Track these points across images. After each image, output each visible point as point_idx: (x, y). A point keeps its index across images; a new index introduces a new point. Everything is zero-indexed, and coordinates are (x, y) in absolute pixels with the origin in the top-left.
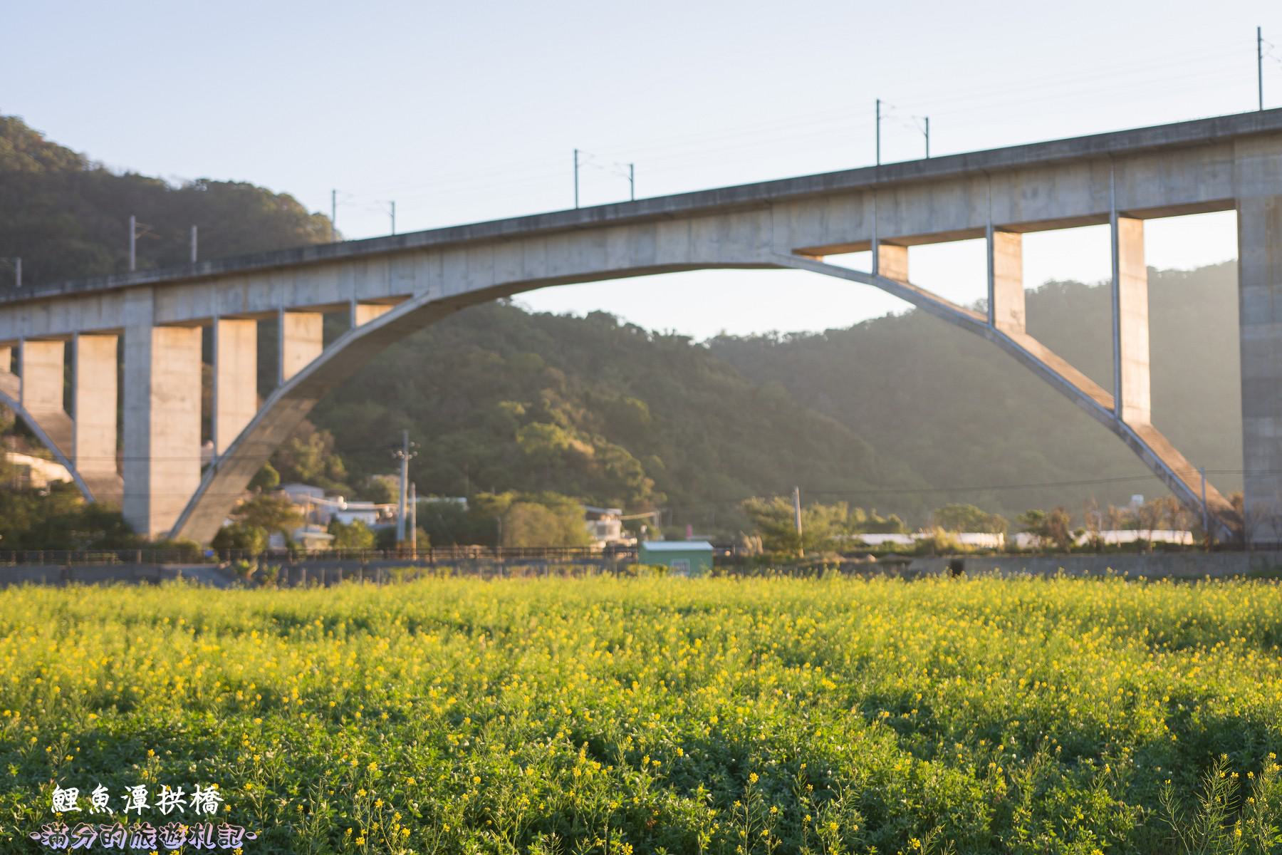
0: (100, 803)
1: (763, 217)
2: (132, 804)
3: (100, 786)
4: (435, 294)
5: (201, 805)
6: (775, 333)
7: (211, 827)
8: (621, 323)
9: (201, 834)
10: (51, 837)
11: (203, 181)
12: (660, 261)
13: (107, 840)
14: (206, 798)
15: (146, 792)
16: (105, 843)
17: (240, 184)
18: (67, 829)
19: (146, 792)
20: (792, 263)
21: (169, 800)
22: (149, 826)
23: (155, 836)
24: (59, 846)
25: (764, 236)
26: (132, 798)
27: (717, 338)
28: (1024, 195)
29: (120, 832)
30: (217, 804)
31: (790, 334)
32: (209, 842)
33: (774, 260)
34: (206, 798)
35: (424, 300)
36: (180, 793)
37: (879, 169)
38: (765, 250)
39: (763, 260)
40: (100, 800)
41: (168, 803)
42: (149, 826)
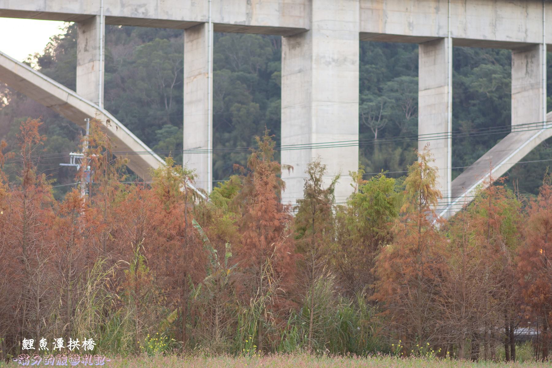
0: (43, 346)
2: (57, 346)
15: (63, 341)
19: (63, 341)
23: (67, 360)
40: (43, 344)
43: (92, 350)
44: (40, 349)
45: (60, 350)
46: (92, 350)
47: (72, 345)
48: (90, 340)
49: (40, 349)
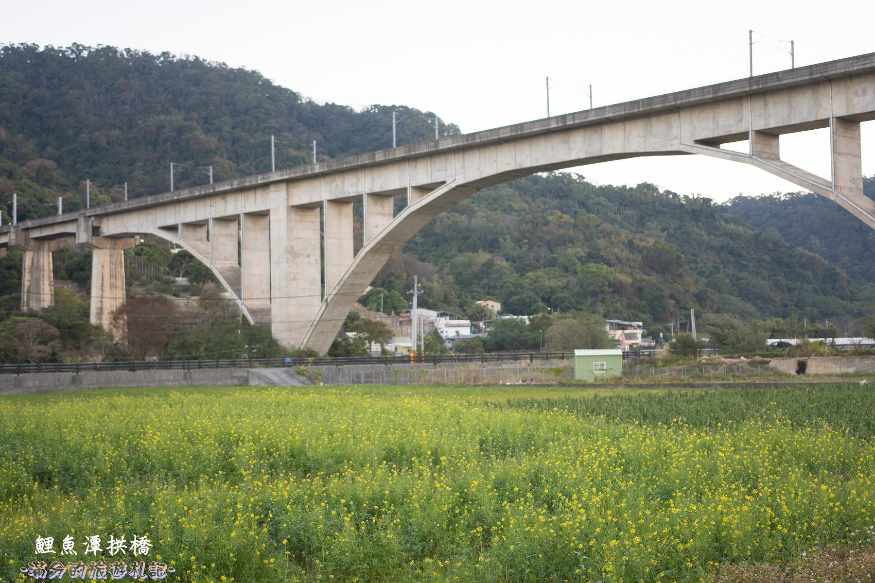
0: (68, 548)
1: (674, 119)
2: (90, 548)
3: (68, 536)
4: (460, 181)
5: (137, 549)
6: (778, 194)
7: (144, 564)
8: (661, 191)
9: (137, 568)
10: (35, 571)
11: (376, 106)
12: (606, 152)
13: (73, 573)
14: (140, 544)
15: (100, 540)
16: (72, 575)
17: (400, 107)
18: (46, 565)
19: (100, 540)
20: (694, 150)
21: (115, 545)
22: (101, 563)
23: (106, 570)
24: (40, 577)
25: (675, 131)
26: (90, 544)
27: (736, 198)
28: (857, 94)
29: (82, 568)
30: (148, 549)
31: (788, 194)
32: (142, 574)
33: (682, 149)
34: (140, 544)
35: (453, 185)
36: (123, 541)
37: (751, 80)
38: (675, 142)
39: (674, 149)
40: (68, 546)
41: (115, 548)
42: (101, 563)
44: (64, 552)
46: (145, 554)
49: (64, 552)
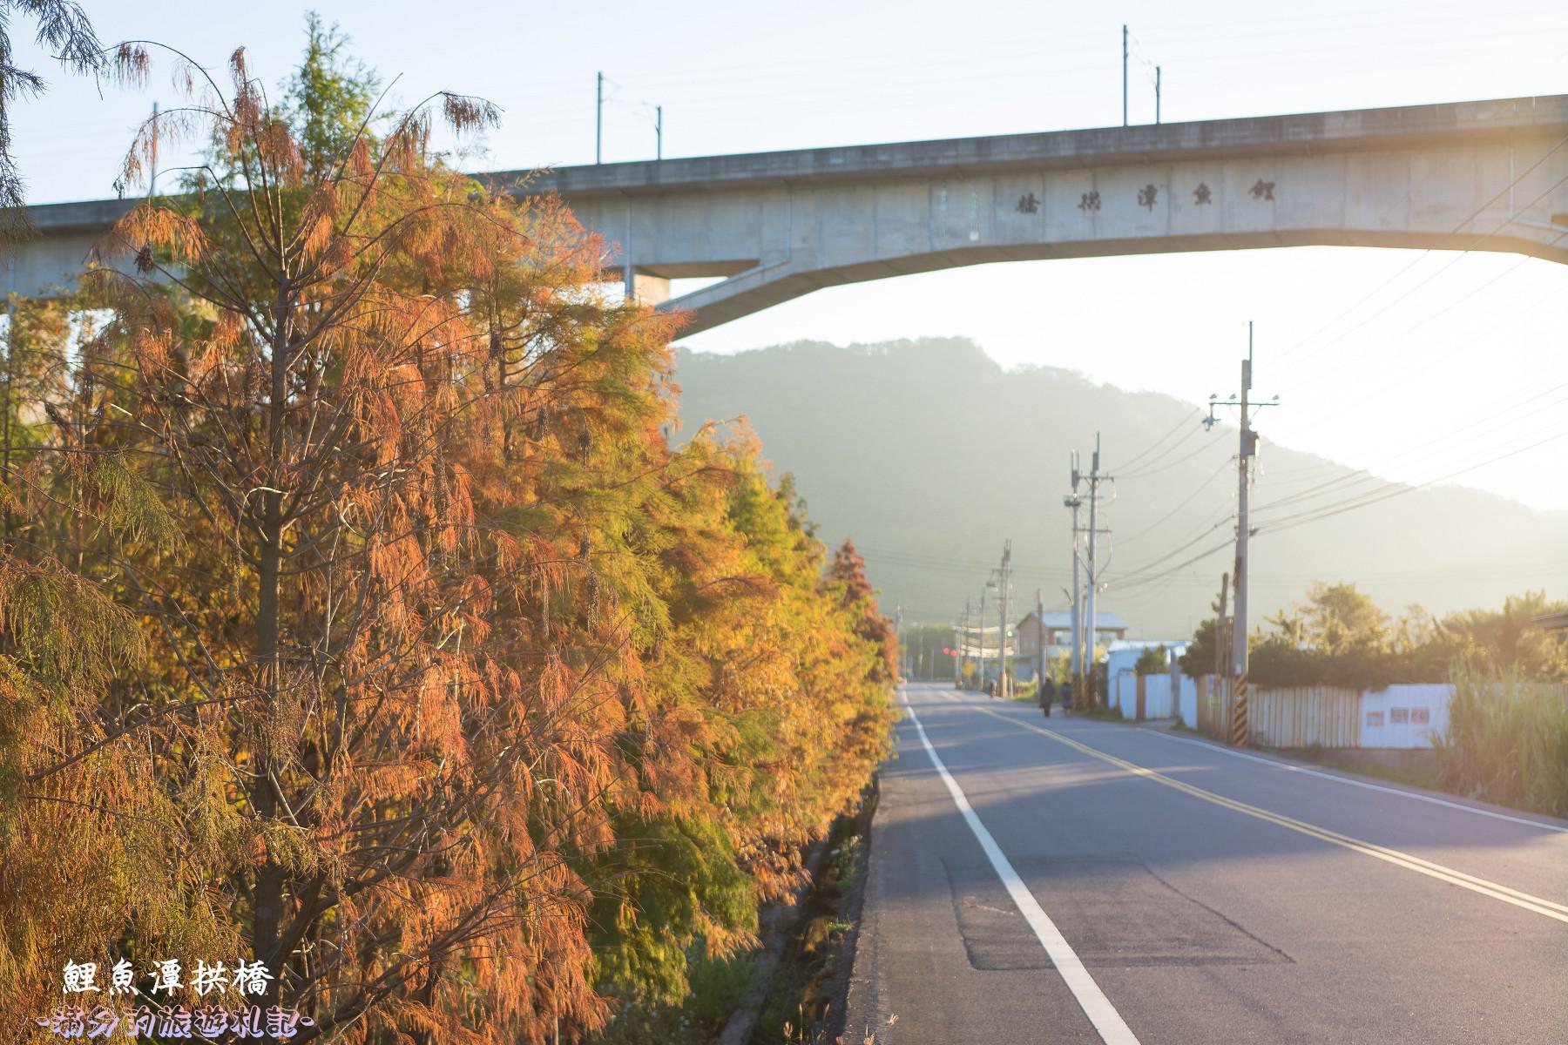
0: (122, 982)
3: (122, 960)
15: (179, 968)
19: (179, 968)
23: (189, 1022)
40: (122, 978)
43: (261, 993)
45: (171, 993)
46: (261, 993)
47: (204, 979)
48: (255, 965)
